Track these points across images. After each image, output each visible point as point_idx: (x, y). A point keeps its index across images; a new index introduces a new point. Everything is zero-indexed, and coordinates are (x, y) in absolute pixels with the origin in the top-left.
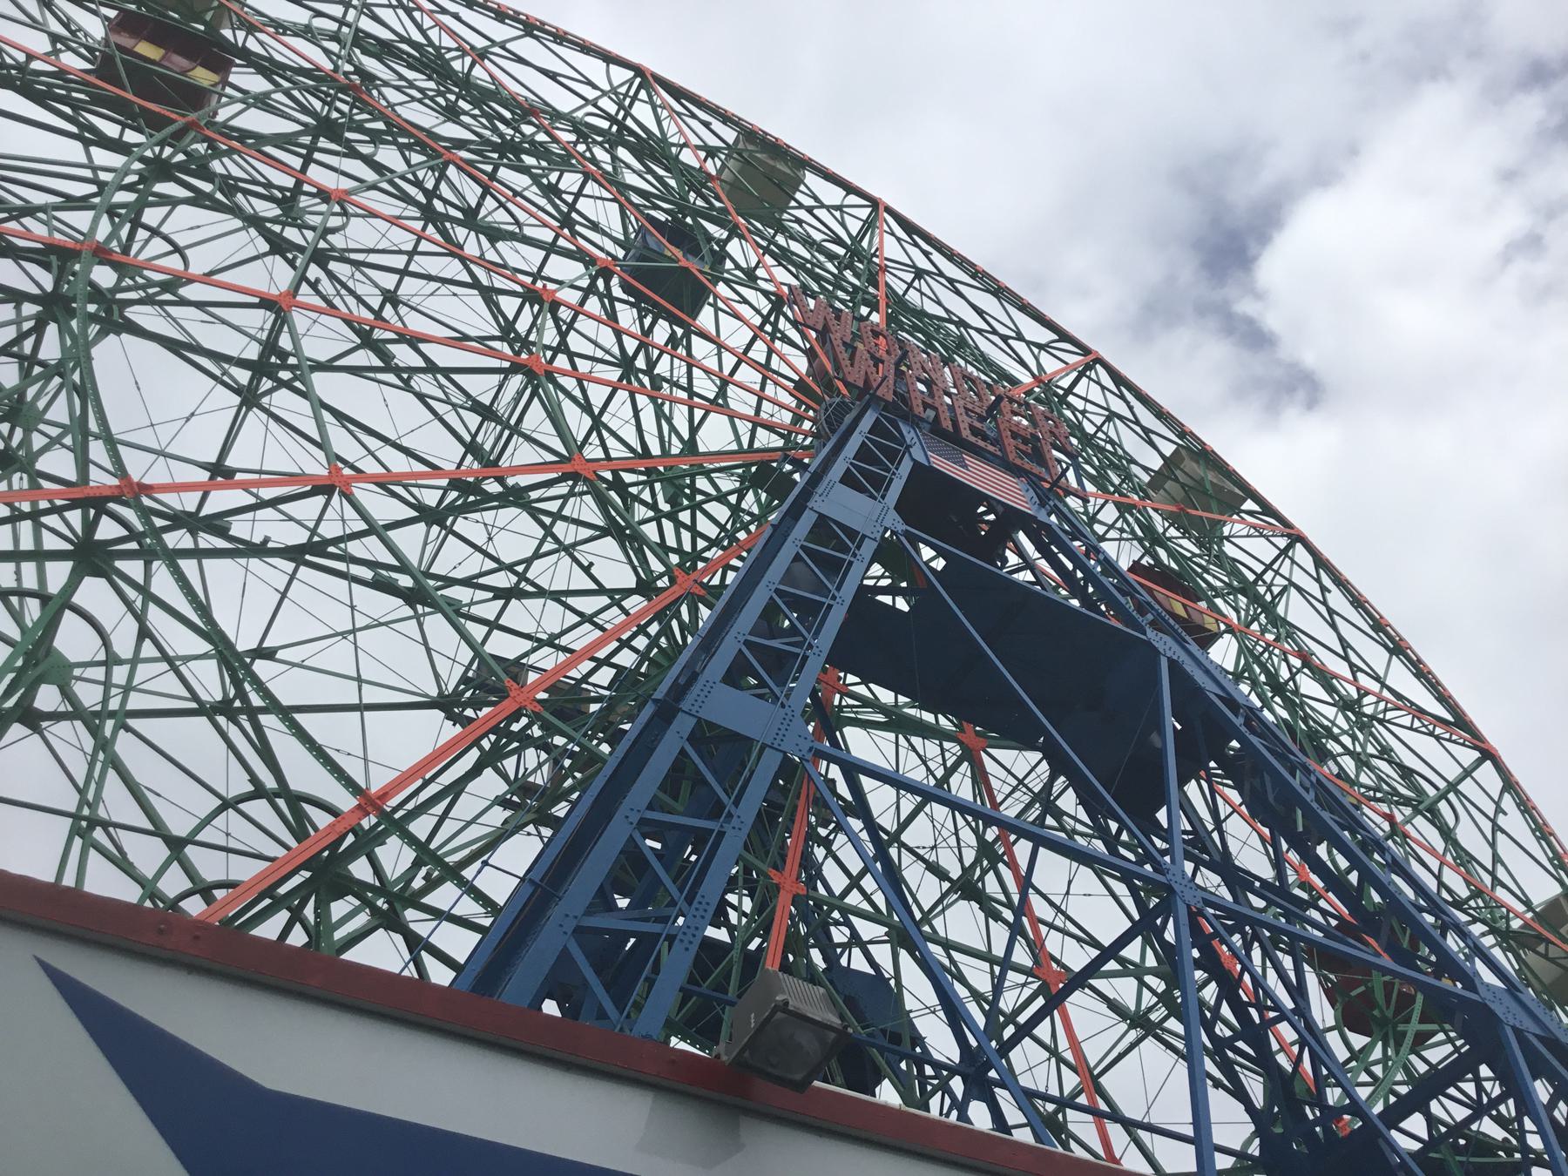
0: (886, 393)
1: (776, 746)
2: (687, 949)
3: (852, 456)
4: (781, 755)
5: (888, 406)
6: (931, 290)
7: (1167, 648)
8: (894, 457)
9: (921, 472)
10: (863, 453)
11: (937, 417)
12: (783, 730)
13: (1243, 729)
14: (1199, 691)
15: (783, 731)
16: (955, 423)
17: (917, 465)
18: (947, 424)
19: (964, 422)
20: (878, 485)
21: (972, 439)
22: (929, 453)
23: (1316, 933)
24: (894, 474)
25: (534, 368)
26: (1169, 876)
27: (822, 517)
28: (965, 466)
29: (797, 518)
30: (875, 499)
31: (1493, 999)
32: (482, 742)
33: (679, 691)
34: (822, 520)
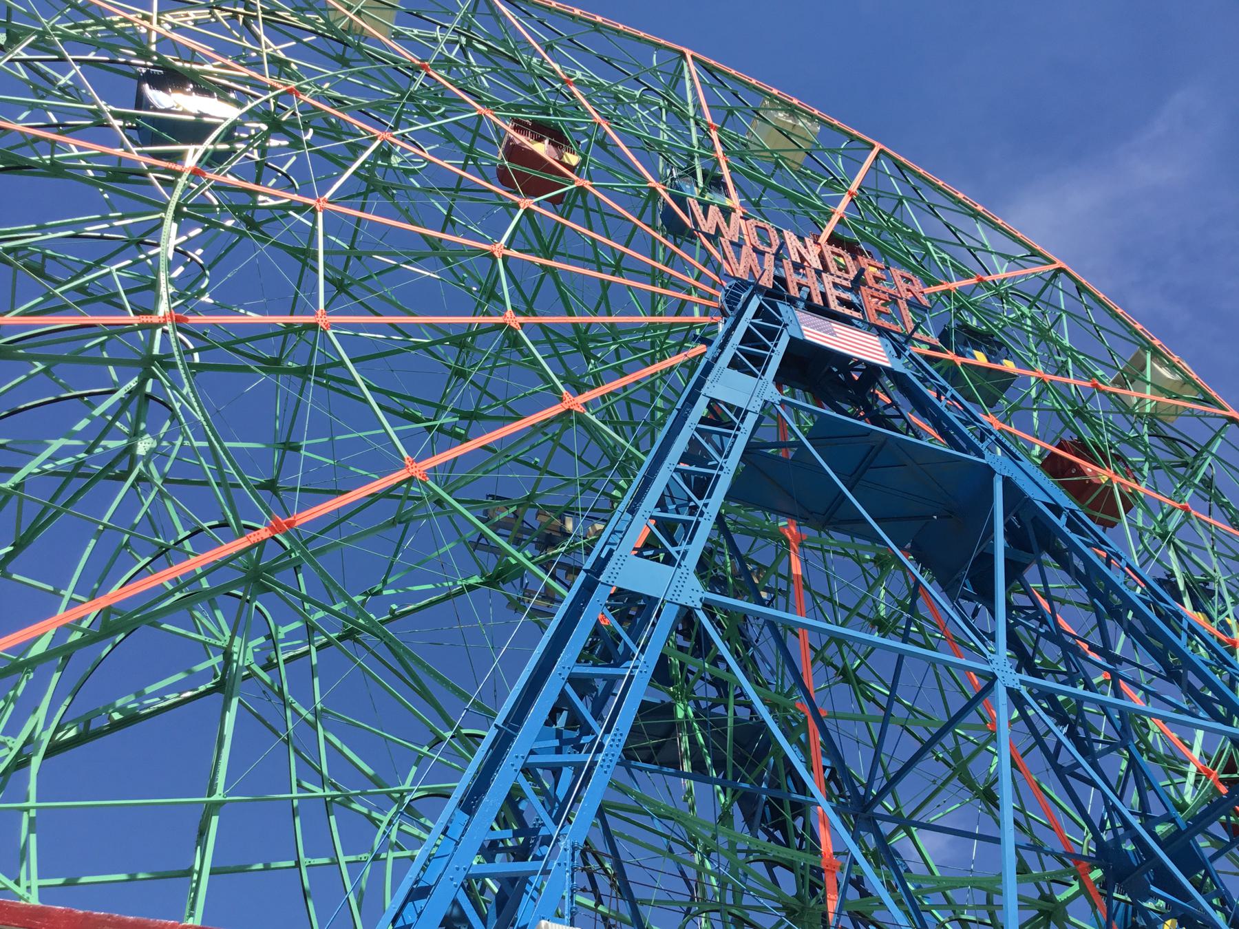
0: (767, 282)
1: (674, 601)
6: (1230, 549)
7: (1003, 467)
8: (772, 335)
9: (797, 345)
10: (748, 338)
11: (809, 295)
13: (1066, 530)
14: (1029, 501)
16: (824, 295)
17: (793, 341)
18: (817, 300)
19: (832, 294)
20: (760, 362)
21: (841, 309)
22: (803, 327)
24: (773, 351)
25: (513, 325)
27: (713, 400)
28: (834, 334)
29: (693, 403)
33: (601, 564)
34: (713, 403)
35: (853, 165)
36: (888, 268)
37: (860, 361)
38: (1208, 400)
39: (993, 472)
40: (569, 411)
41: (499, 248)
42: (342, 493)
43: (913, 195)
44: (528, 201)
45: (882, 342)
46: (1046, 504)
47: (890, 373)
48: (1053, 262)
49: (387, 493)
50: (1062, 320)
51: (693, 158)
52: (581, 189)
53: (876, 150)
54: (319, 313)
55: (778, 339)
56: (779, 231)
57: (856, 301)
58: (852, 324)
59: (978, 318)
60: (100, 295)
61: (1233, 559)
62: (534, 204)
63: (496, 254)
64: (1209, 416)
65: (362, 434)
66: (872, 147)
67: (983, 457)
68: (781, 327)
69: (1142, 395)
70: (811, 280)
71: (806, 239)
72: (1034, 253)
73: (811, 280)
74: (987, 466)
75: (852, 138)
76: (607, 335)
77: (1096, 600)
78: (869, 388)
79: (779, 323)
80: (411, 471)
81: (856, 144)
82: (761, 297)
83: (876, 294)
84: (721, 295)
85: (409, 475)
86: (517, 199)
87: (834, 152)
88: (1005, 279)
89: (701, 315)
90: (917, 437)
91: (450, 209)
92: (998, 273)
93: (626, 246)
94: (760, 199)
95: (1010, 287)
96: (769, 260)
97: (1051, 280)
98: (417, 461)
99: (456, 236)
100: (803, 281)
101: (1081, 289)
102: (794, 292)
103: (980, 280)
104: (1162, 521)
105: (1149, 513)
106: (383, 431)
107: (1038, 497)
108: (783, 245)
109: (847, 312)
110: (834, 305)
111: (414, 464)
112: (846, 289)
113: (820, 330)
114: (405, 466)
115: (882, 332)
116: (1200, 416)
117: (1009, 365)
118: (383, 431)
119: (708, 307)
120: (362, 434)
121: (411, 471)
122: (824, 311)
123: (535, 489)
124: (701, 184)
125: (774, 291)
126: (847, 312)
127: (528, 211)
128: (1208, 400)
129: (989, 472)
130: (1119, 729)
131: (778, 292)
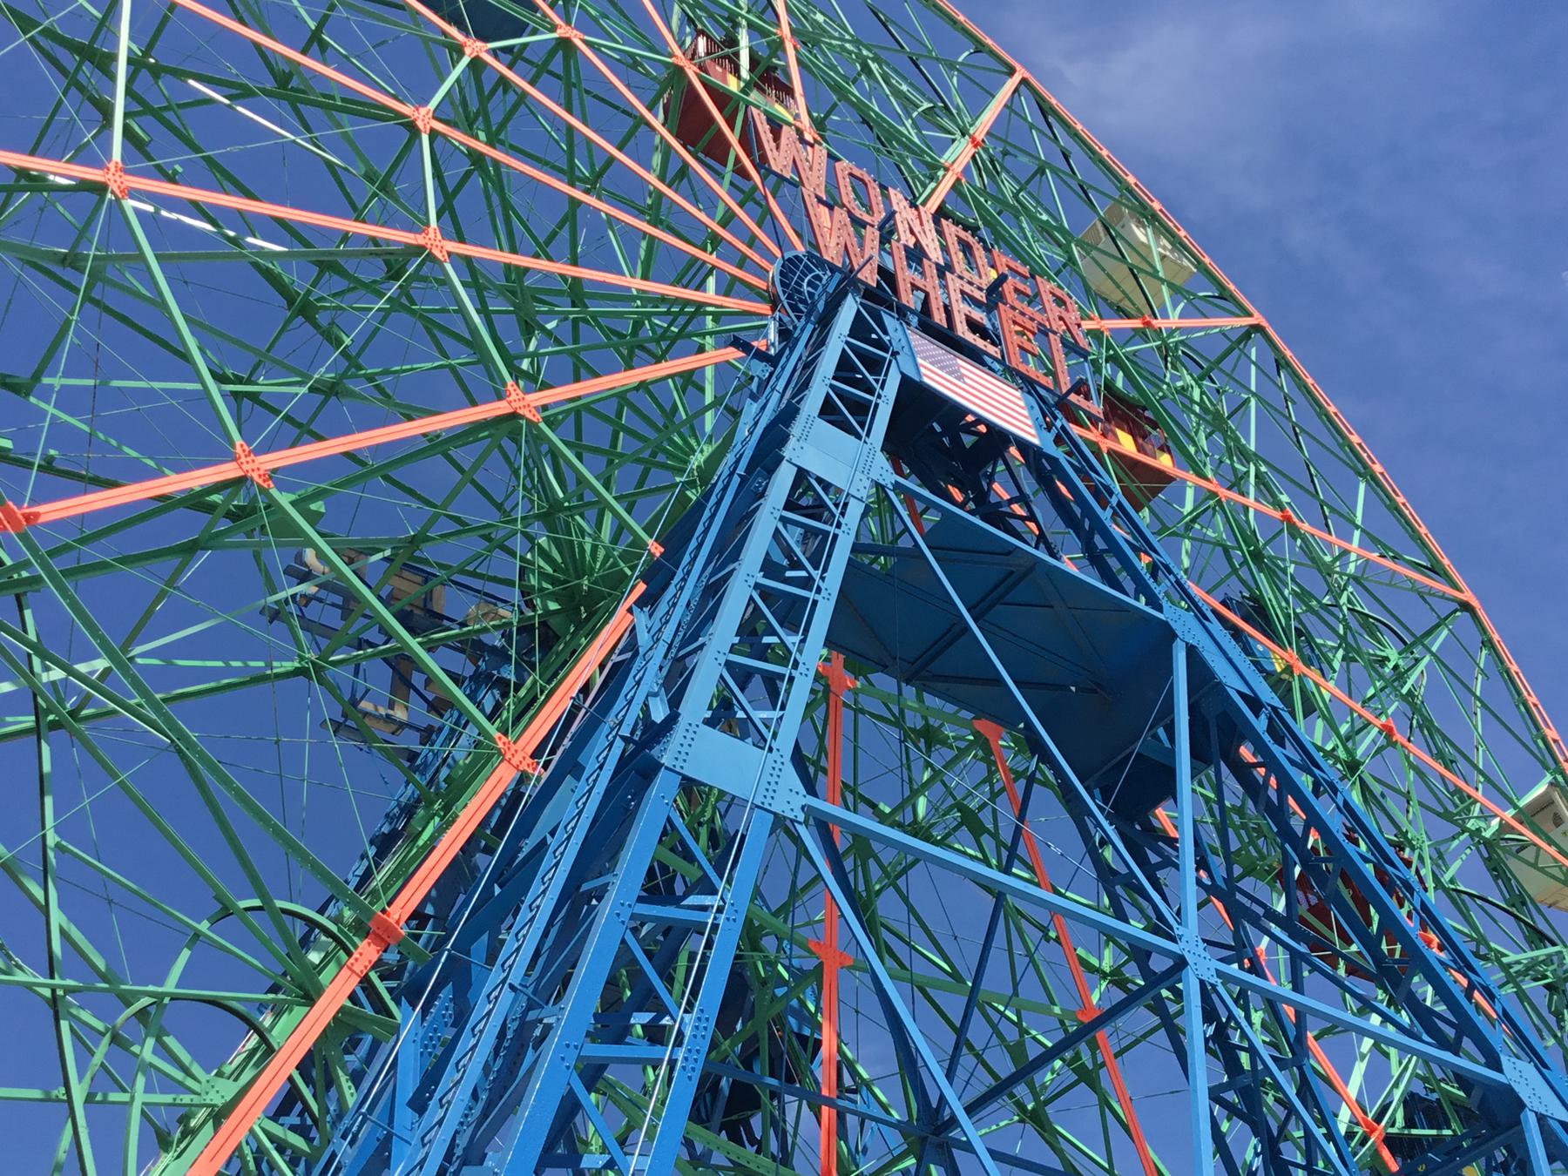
0: (870, 277)
1: (766, 806)
2: (690, 1078)
3: (831, 374)
4: (771, 817)
5: (869, 294)
8: (875, 365)
12: (686, 745)
14: (1220, 687)
15: (773, 786)
18: (939, 318)
19: (961, 310)
22: (920, 361)
23: (1025, 225)
25: (436, 252)
26: (1182, 944)
28: (960, 378)
30: (859, 437)
31: (1518, 1079)
32: (1366, 1039)
35: (980, 95)
36: (1033, 277)
37: (980, 420)
38: (1435, 570)
39: (1173, 636)
40: (514, 416)
41: (423, 116)
42: (113, 485)
43: (1060, 163)
44: (479, 44)
45: (1027, 404)
46: (1239, 693)
47: (1024, 446)
48: (1250, 315)
49: (196, 501)
50: (1248, 408)
51: (736, 25)
52: (565, 43)
53: (1017, 78)
54: (112, 166)
55: (886, 375)
56: (883, 188)
57: (986, 322)
58: (983, 363)
59: (1128, 375)
60: (1359, 609)
61: (1439, 814)
62: (488, 51)
63: (420, 124)
64: (1434, 595)
65: (157, 385)
66: (1011, 72)
67: (1160, 610)
68: (888, 356)
69: (1345, 545)
70: (931, 283)
71: (892, 191)
72: (1224, 295)
73: (931, 283)
74: (1166, 624)
75: (980, 47)
76: (560, 293)
77: (1287, 846)
78: (985, 464)
79: (885, 348)
80: (245, 467)
81: (983, 58)
82: (858, 300)
83: (1019, 319)
84: (774, 270)
85: (240, 473)
86: (460, 37)
87: (951, 66)
88: (1177, 329)
89: (717, 293)
90: (1053, 554)
91: (322, 22)
92: (1168, 317)
93: (620, 149)
94: (827, 116)
95: (1182, 342)
96: (872, 235)
97: (1239, 342)
98: (258, 451)
99: (325, 64)
100: (920, 282)
101: (1281, 364)
102: (911, 300)
103: (1148, 324)
104: (1348, 738)
105: (1332, 726)
106: (198, 386)
107: (1231, 682)
108: (891, 215)
109: (980, 343)
110: (962, 330)
111: (252, 457)
112: (976, 303)
113: (941, 368)
114: (235, 459)
115: (1028, 385)
116: (1423, 595)
117: (1165, 462)
118: (198, 386)
119: (735, 278)
120: (157, 385)
121: (245, 467)
122: (946, 337)
123: (427, 527)
124: (745, 74)
125: (878, 292)
126: (980, 343)
127: (476, 64)
128: (1435, 570)
129: (1168, 634)
130: (1292, 1040)
131: (882, 296)
